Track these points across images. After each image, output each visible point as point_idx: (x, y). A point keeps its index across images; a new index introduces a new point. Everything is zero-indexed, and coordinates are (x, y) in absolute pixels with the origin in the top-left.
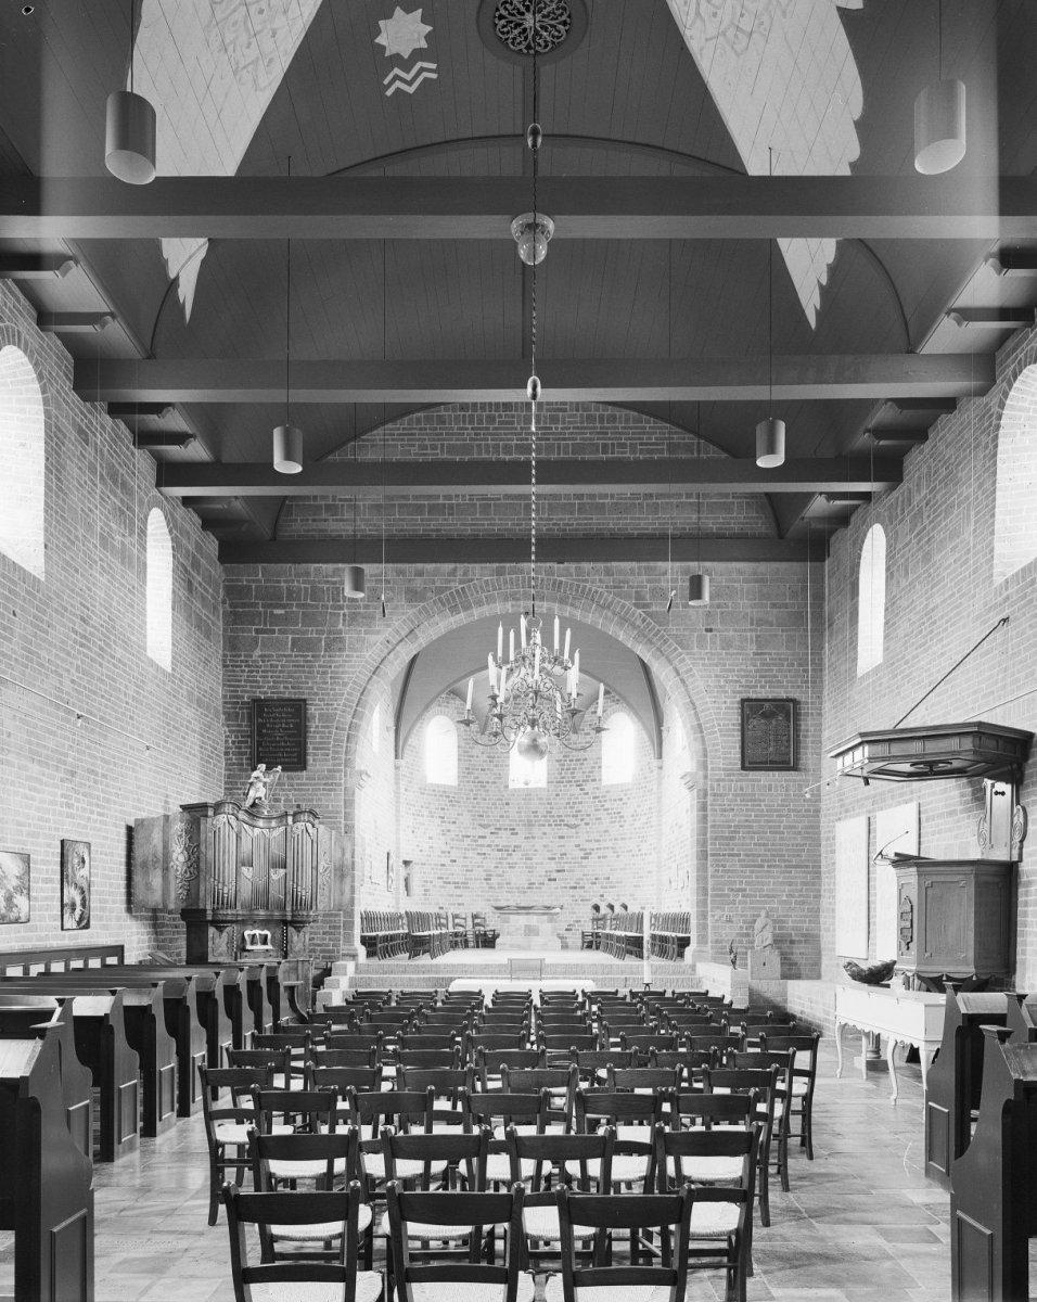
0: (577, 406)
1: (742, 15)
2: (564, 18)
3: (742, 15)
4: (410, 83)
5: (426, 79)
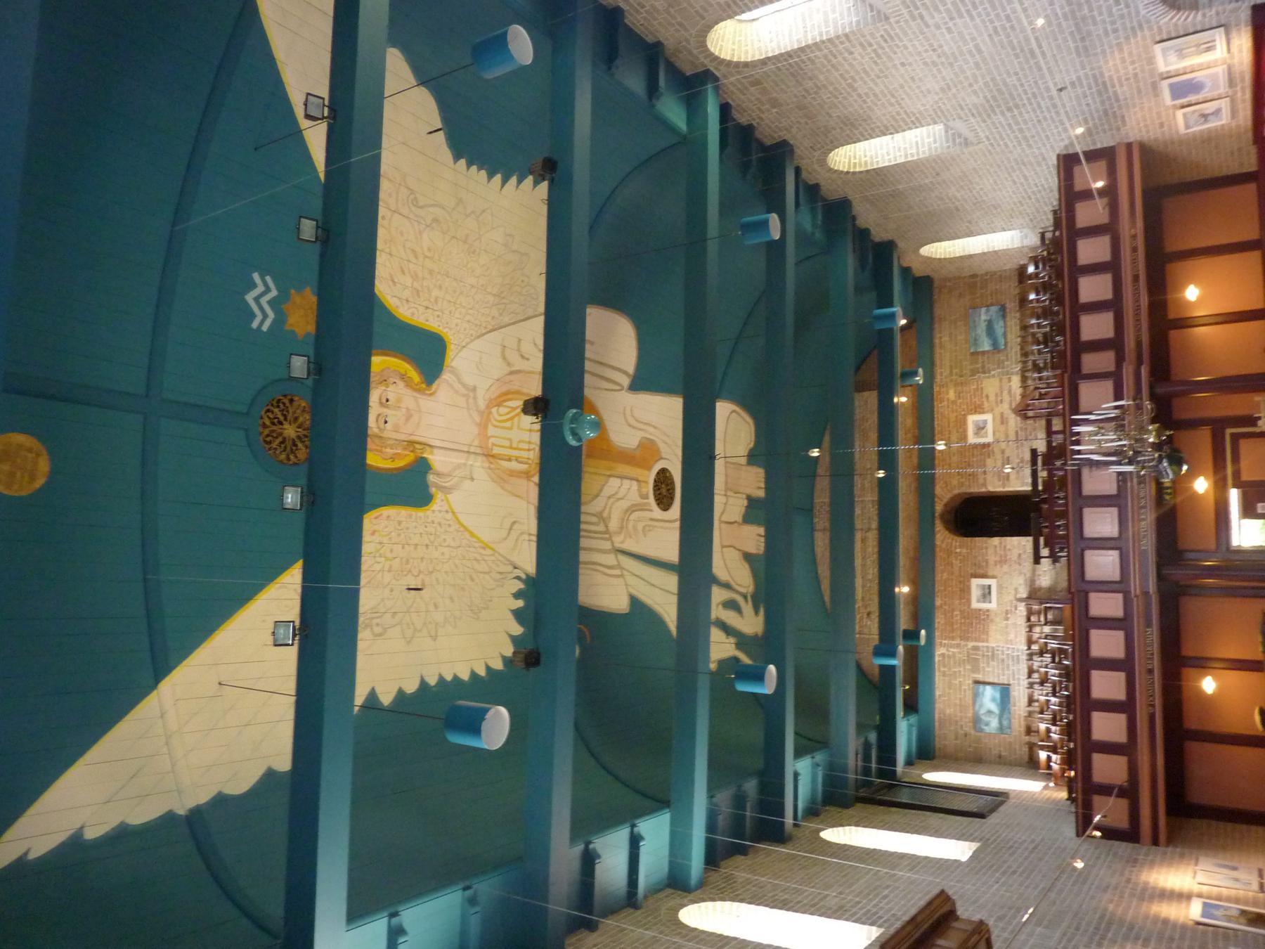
0: (1254, 933)
2: (286, 401)
4: (257, 299)
5: (253, 316)
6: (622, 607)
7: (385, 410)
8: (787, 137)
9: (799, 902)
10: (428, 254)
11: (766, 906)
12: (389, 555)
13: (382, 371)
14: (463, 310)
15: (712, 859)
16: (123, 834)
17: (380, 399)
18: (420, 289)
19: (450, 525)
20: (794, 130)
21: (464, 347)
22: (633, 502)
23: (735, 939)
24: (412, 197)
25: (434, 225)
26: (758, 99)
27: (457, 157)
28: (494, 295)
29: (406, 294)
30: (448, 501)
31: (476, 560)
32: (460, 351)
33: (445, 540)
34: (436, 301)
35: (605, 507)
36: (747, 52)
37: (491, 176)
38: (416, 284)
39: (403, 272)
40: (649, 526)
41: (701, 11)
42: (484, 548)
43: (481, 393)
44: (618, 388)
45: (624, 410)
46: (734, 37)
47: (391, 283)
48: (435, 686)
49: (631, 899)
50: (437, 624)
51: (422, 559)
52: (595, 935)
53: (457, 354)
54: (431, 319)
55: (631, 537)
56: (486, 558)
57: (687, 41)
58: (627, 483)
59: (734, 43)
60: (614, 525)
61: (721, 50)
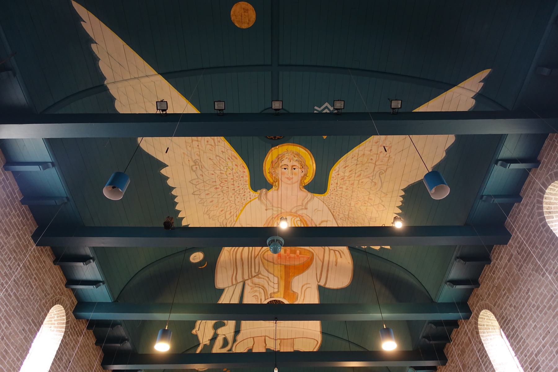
1: (198, 146)
3: (198, 146)
4: (326, 107)
6: (218, 285)
7: (290, 168)
8: (449, 361)
9: (59, 366)
10: (360, 181)
11: (59, 349)
12: (228, 172)
13: (307, 166)
14: (339, 201)
15: (92, 325)
16: (95, 59)
17: (294, 166)
18: (345, 180)
19: (244, 200)
20: (453, 365)
21: (324, 202)
22: (267, 290)
23: (38, 330)
24: (383, 172)
25: (373, 183)
26: (463, 342)
27: (405, 190)
28: (348, 215)
29: (342, 174)
30: (255, 199)
31: (231, 213)
32: (321, 200)
33: (238, 198)
34: (341, 188)
35: (263, 275)
36: (484, 333)
37: (400, 207)
38: (346, 178)
39: (350, 171)
40: (258, 299)
41: (497, 304)
42: (236, 216)
43: (304, 211)
44: (318, 280)
45: (309, 284)
46: (490, 326)
47: (345, 166)
48: (171, 194)
49: (71, 281)
50: (200, 195)
51: (228, 188)
52: (52, 263)
53: (320, 199)
54: (333, 186)
55: (251, 289)
56: (232, 217)
57: (482, 300)
58: (276, 286)
59: (487, 325)
60: (256, 280)
61: (482, 318)
